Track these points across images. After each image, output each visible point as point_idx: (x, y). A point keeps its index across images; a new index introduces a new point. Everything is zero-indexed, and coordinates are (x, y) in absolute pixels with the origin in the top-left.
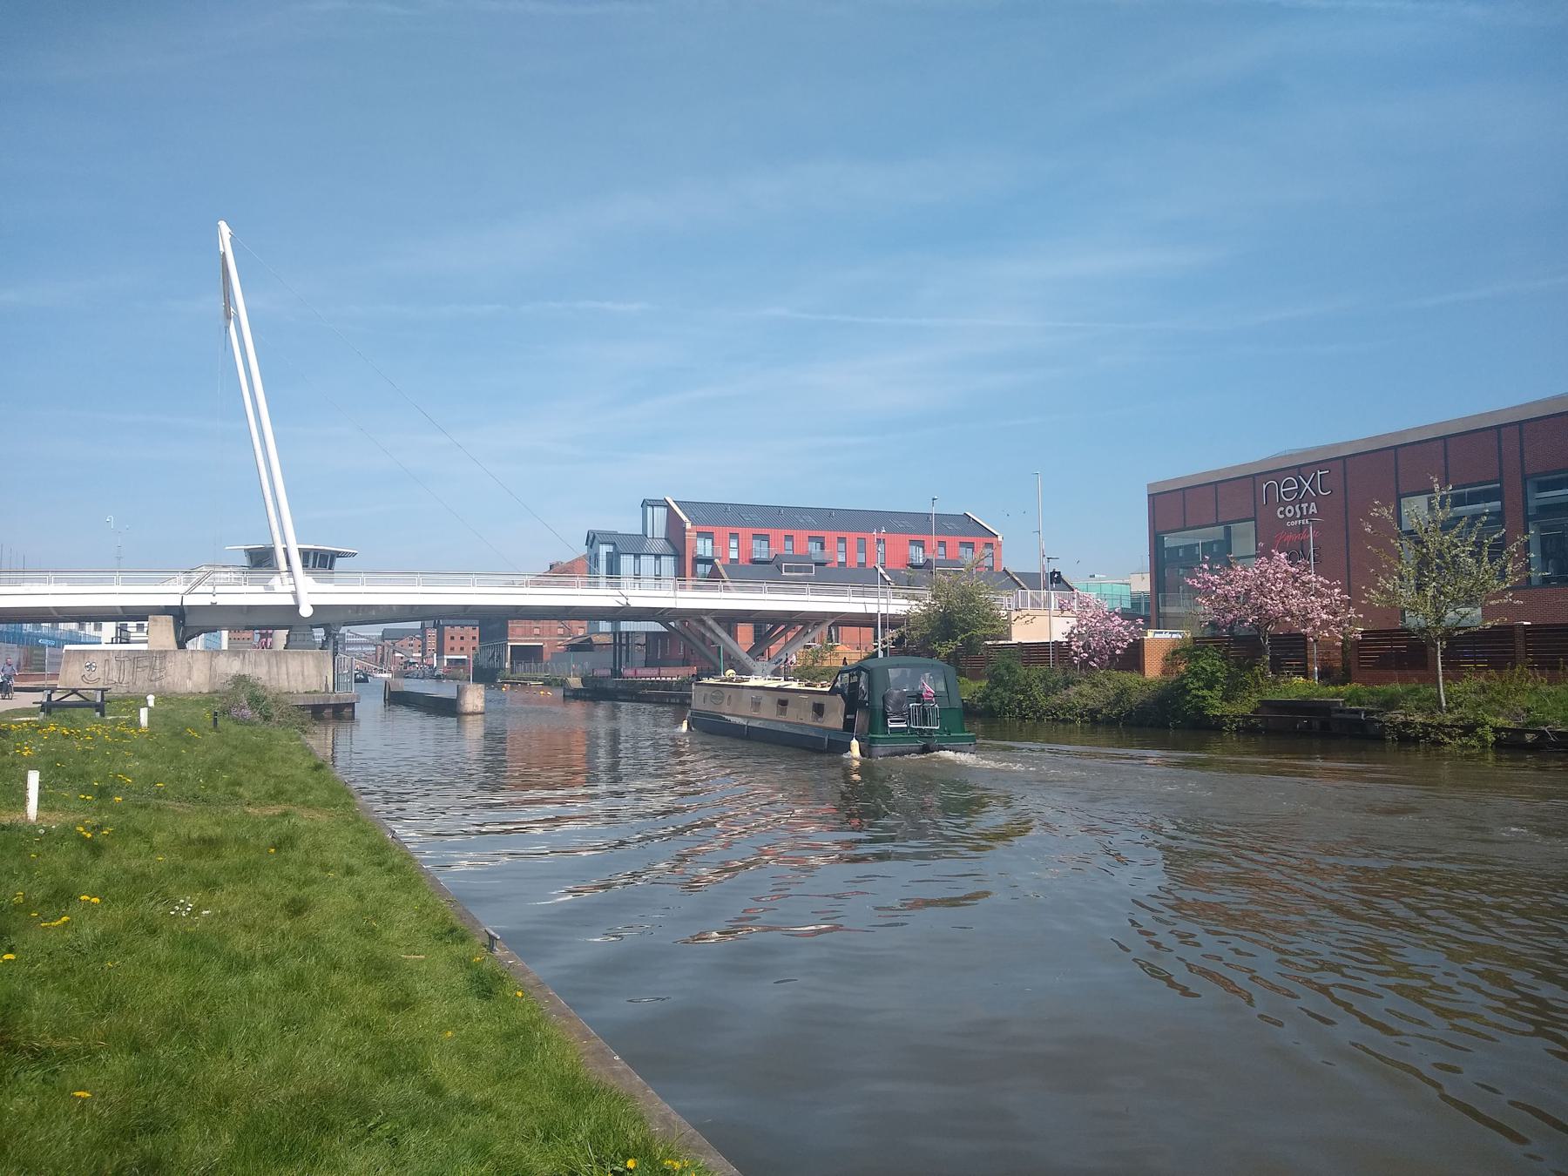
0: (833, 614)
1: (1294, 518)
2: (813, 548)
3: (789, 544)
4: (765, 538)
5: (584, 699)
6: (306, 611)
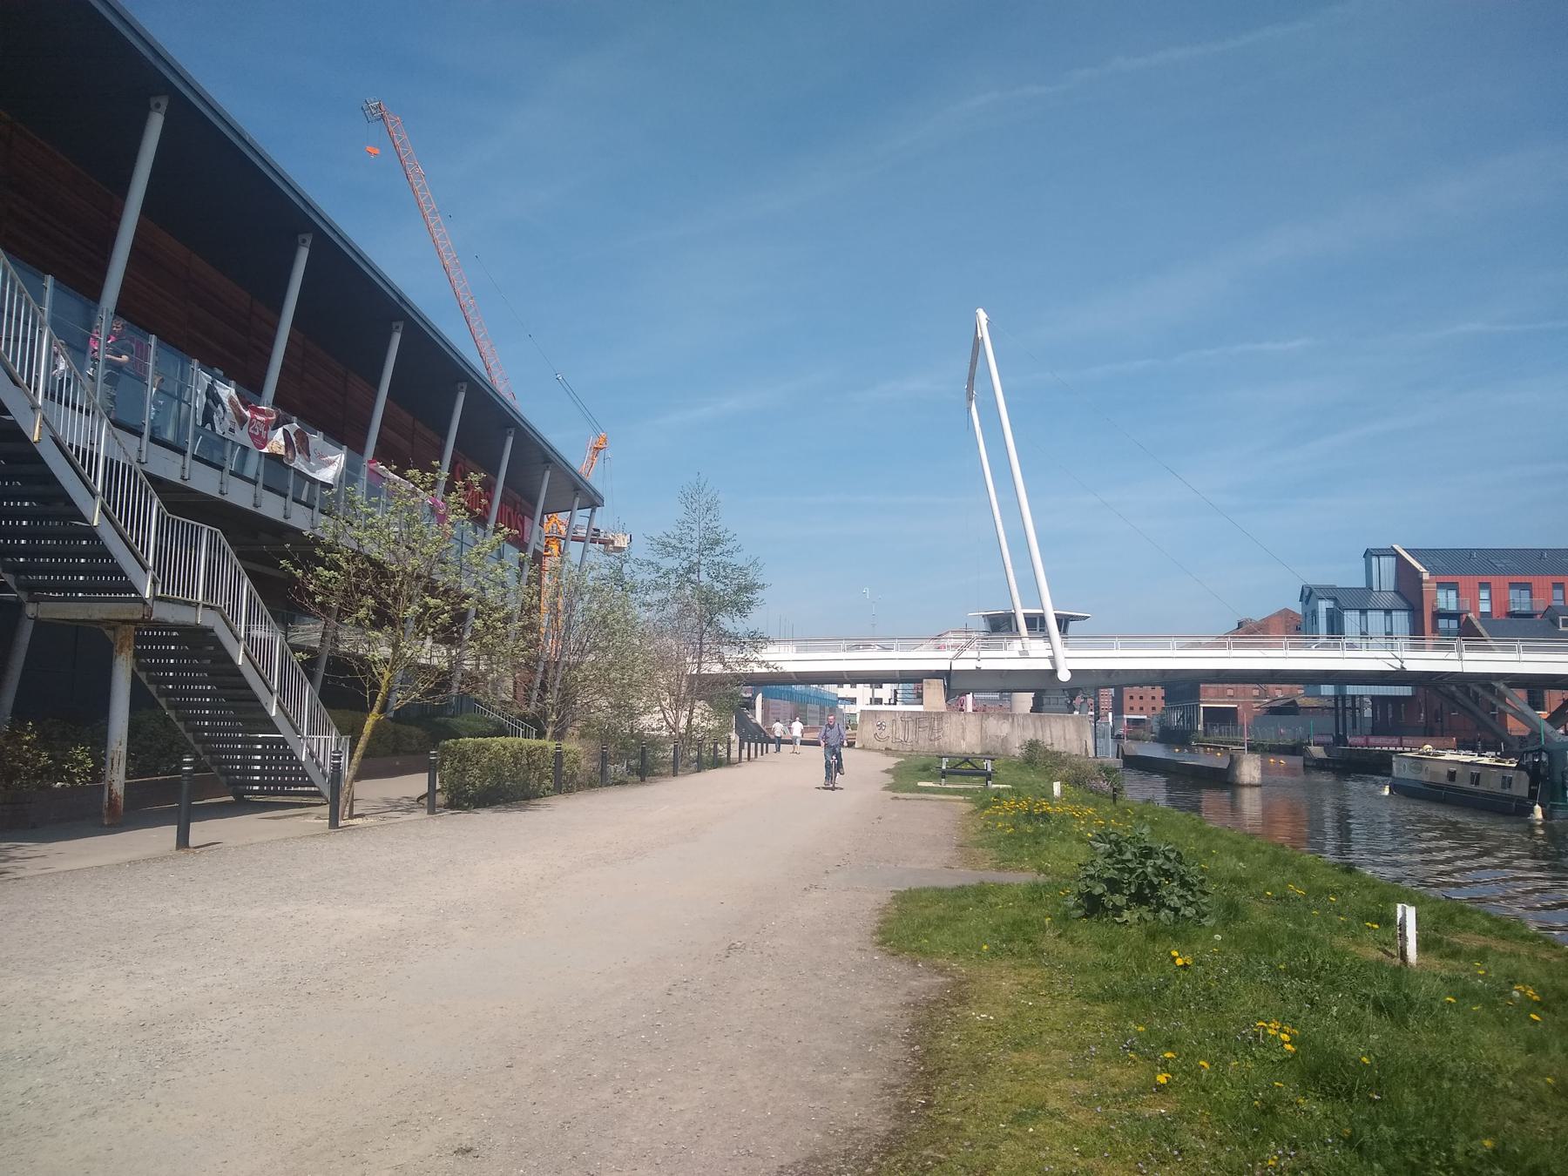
3: (1558, 594)
4: (1526, 586)
5: (1333, 770)
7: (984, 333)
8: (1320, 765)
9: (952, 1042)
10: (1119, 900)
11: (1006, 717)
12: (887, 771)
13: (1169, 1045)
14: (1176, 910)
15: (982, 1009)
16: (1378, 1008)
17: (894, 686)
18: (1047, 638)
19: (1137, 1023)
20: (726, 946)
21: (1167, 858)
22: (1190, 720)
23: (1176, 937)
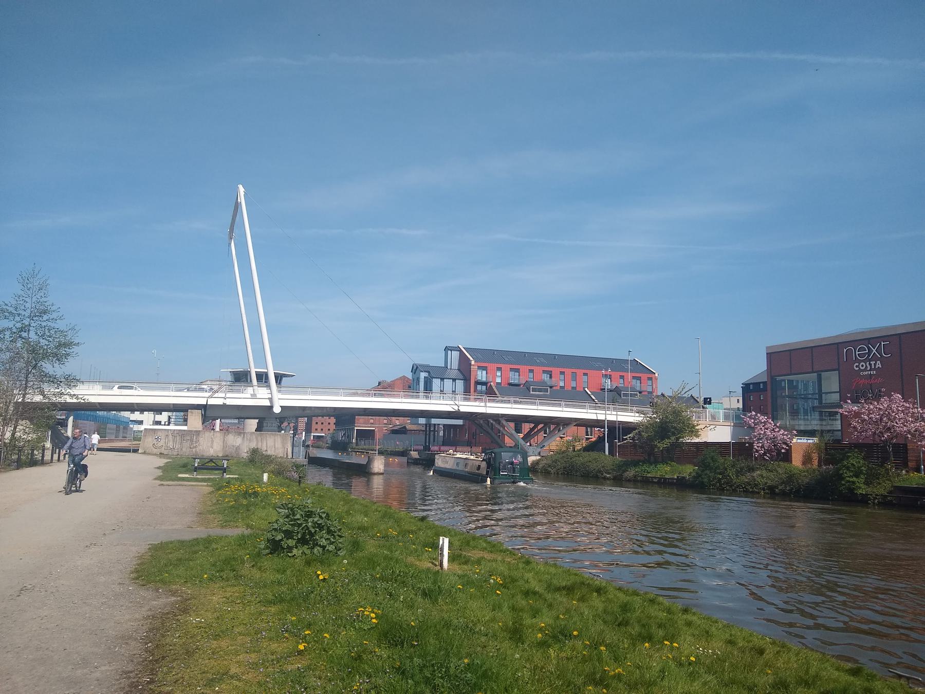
0: (576, 420)
1: (866, 370)
2: (545, 377)
3: (531, 375)
4: (517, 370)
6: (277, 410)
7: (242, 199)
8: (416, 462)
9: (174, 639)
10: (291, 543)
11: (240, 434)
12: (159, 468)
13: (309, 626)
14: (324, 547)
15: (198, 616)
16: (425, 594)
17: (170, 414)
18: (269, 387)
19: (292, 615)
20: (19, 588)
21: (321, 517)
22: (348, 437)
23: (322, 562)
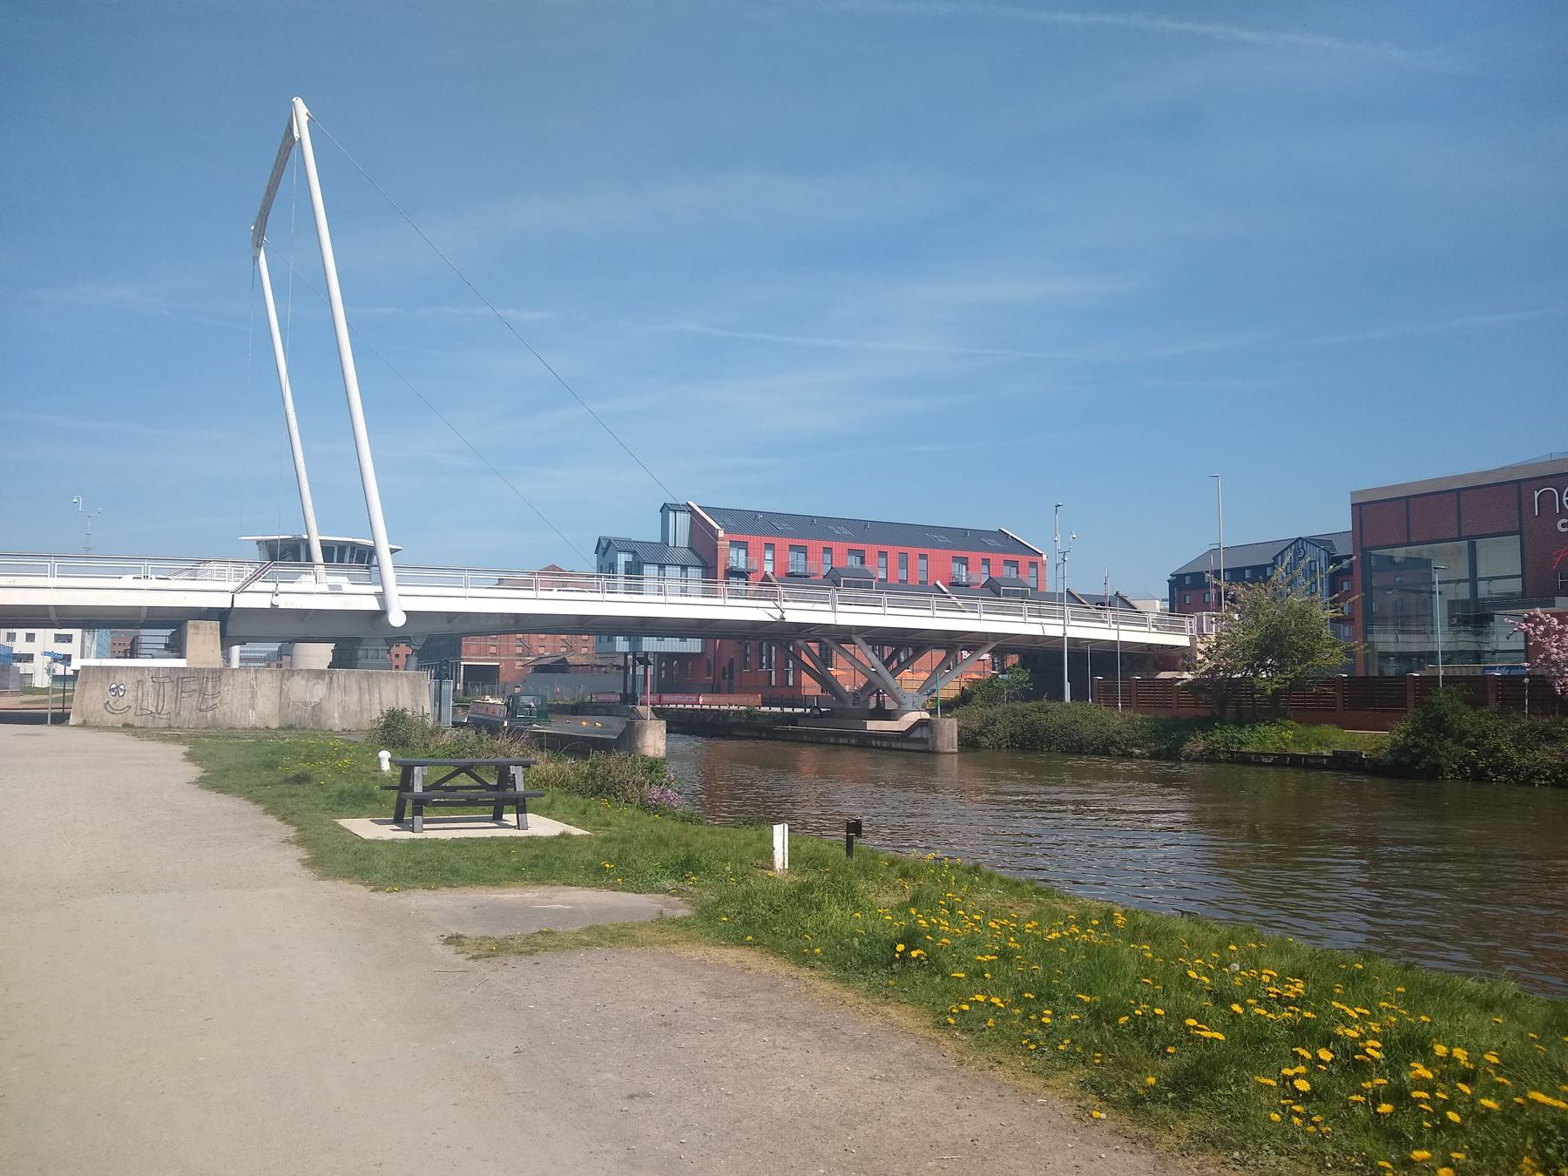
2: (853, 562)
4: (802, 549)
6: (397, 619)
7: (302, 130)
